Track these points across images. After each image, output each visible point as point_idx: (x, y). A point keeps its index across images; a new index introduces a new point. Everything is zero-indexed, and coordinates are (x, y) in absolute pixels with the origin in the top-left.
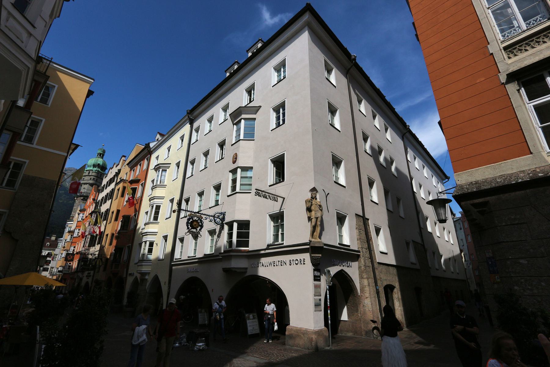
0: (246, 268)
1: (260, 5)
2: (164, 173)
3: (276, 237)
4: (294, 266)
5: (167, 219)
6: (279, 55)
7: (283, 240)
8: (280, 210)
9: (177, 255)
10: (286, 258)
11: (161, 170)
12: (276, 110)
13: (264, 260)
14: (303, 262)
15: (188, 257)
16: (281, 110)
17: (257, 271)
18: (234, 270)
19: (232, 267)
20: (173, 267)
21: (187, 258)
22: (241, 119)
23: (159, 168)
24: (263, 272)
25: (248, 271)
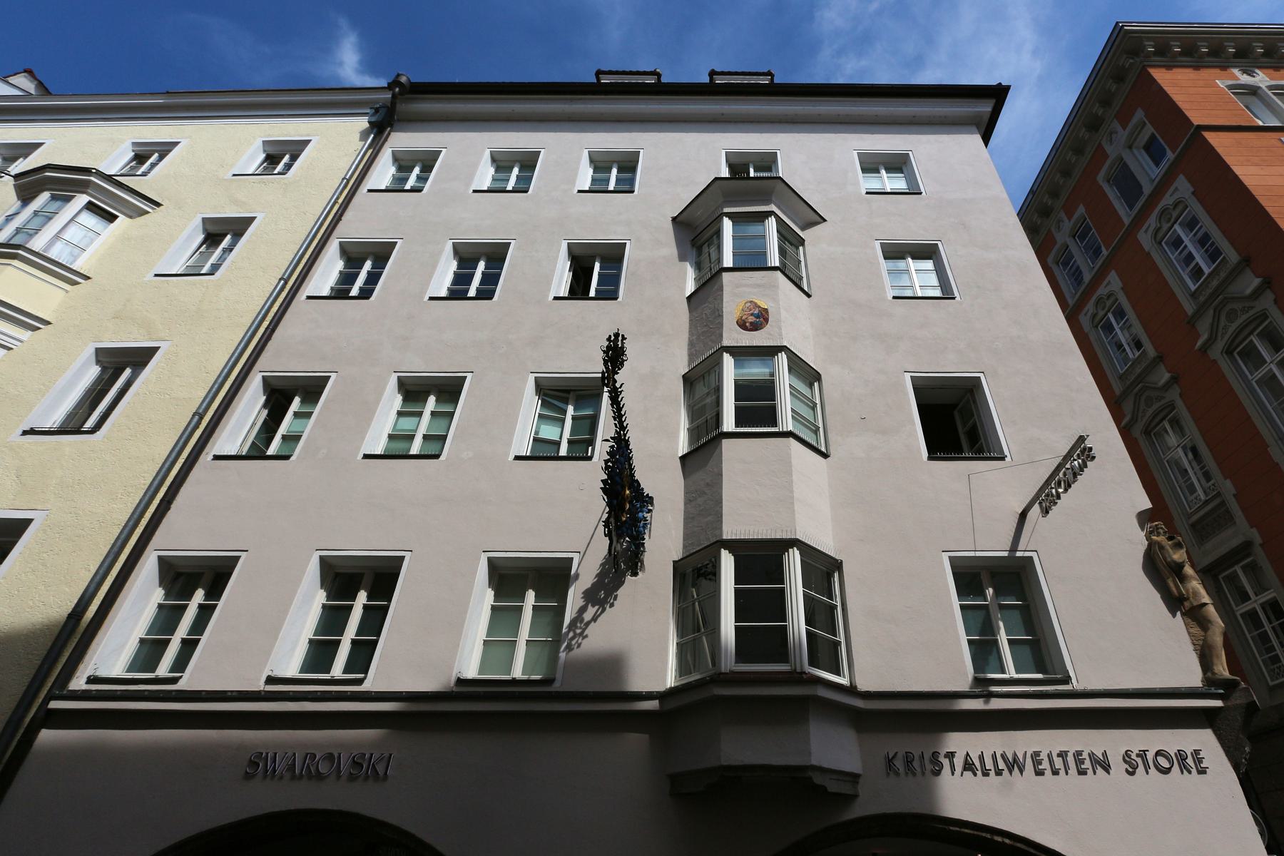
0: (854, 778)
1: (343, 22)
2: (89, 219)
3: (321, 653)
4: (1148, 780)
5: (32, 432)
6: (662, 135)
7: (181, 664)
8: (1014, 548)
9: (112, 655)
10: (1114, 742)
11: (82, 199)
12: (466, 257)
13: (960, 743)
14: (1189, 763)
15: (271, 680)
16: (368, 265)
17: (929, 793)
18: (818, 779)
19: (814, 762)
20: (47, 736)
21: (260, 685)
22: (772, 213)
23: (83, 187)
24: (964, 798)
25: (863, 790)
